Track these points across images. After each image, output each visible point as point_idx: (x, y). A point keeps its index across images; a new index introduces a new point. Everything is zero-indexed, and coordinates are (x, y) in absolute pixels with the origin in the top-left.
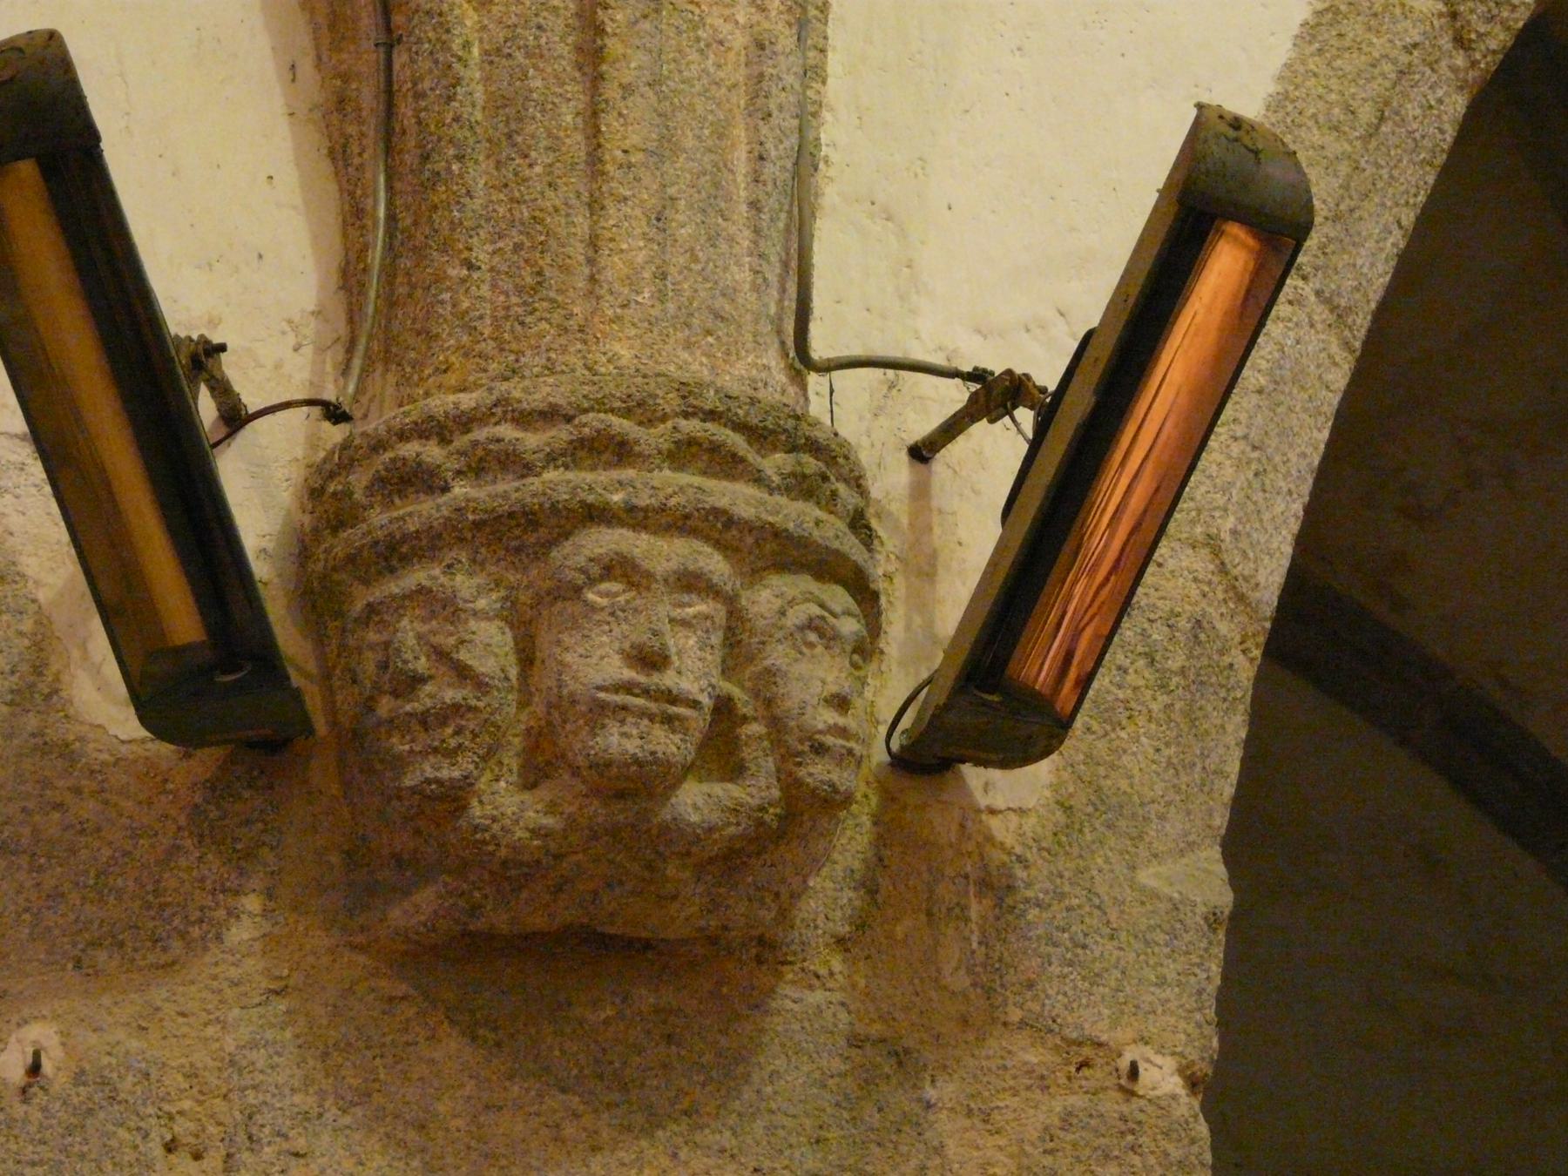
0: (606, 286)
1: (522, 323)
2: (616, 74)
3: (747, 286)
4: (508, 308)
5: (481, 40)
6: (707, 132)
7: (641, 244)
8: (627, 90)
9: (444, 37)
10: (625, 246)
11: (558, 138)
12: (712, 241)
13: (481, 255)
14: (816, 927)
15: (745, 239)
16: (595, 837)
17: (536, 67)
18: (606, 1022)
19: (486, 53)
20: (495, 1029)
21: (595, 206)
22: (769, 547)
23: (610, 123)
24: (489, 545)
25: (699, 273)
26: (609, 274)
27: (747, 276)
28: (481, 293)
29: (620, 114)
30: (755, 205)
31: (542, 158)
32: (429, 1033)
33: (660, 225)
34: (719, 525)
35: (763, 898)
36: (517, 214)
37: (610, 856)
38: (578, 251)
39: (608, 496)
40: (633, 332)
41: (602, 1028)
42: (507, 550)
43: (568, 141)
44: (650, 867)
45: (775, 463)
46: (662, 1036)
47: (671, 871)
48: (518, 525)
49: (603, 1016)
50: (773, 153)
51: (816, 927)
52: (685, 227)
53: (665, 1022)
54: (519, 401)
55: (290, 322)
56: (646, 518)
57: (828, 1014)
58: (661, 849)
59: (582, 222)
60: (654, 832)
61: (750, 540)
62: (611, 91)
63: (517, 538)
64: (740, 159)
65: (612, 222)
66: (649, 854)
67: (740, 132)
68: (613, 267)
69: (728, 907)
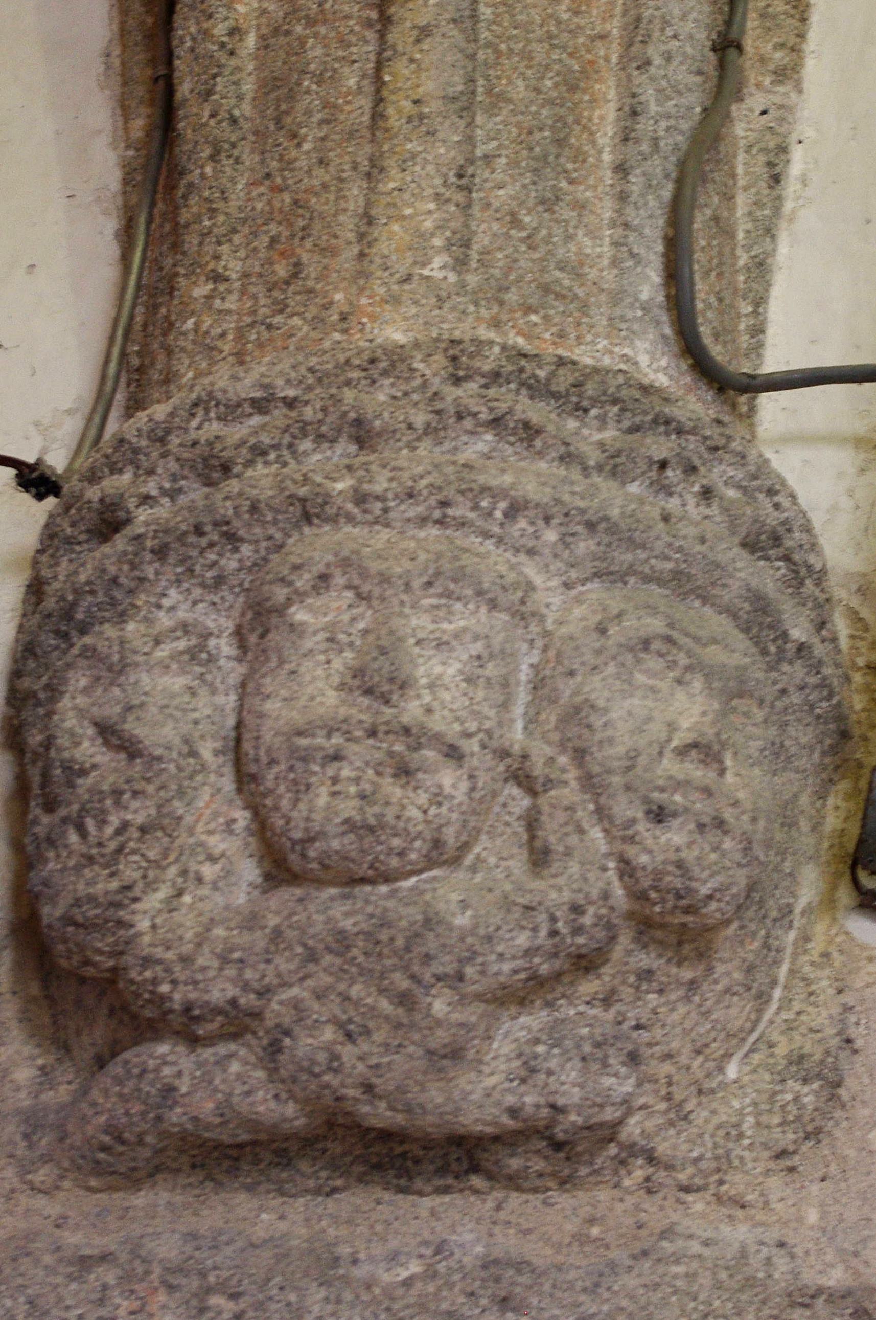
0: (378, 261)
1: (269, 327)
2: (408, 15)
3: (606, 262)
4: (254, 312)
5: (258, 27)
6: (549, 83)
7: (432, 206)
8: (425, 32)
9: (206, 25)
10: (408, 211)
11: (335, 106)
12: (549, 203)
13: (233, 266)
14: (741, 1136)
15: (606, 210)
16: (312, 957)
17: (316, 35)
18: (408, 1283)
19: (263, 38)
20: (234, 1296)
21: (374, 171)
22: (585, 546)
23: (399, 73)
24: (179, 582)
25: (522, 240)
26: (383, 247)
27: (606, 249)
28: (227, 305)
29: (412, 60)
30: (622, 169)
31: (311, 135)
32: (136, 1304)
33: (464, 181)
34: (498, 514)
35: (606, 1056)
36: (277, 205)
37: (342, 987)
38: (347, 226)
39: (328, 484)
40: (414, 310)
41: (400, 1291)
42: (203, 585)
43: (348, 108)
44: (404, 1000)
45: (594, 435)
46: (493, 1297)
47: (439, 1007)
48: (211, 545)
49: (404, 1274)
50: (653, 108)
51: (741, 1136)
52: (502, 187)
53: (497, 1280)
54: (225, 391)
55: (37, 424)
56: (386, 510)
57: (756, 1261)
58: (416, 968)
59: (355, 192)
60: (400, 942)
61: (551, 536)
62: (399, 36)
63: (214, 564)
64: (606, 119)
65: (392, 185)
66: (401, 982)
67: (609, 90)
68: (391, 238)
69: (550, 1073)
